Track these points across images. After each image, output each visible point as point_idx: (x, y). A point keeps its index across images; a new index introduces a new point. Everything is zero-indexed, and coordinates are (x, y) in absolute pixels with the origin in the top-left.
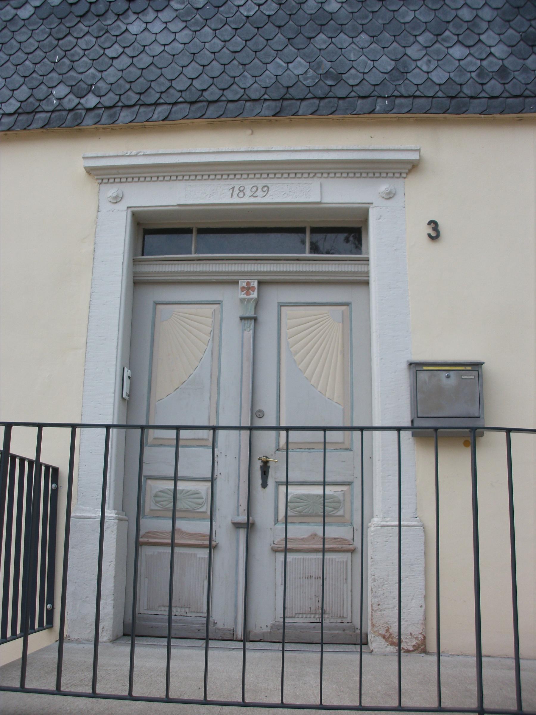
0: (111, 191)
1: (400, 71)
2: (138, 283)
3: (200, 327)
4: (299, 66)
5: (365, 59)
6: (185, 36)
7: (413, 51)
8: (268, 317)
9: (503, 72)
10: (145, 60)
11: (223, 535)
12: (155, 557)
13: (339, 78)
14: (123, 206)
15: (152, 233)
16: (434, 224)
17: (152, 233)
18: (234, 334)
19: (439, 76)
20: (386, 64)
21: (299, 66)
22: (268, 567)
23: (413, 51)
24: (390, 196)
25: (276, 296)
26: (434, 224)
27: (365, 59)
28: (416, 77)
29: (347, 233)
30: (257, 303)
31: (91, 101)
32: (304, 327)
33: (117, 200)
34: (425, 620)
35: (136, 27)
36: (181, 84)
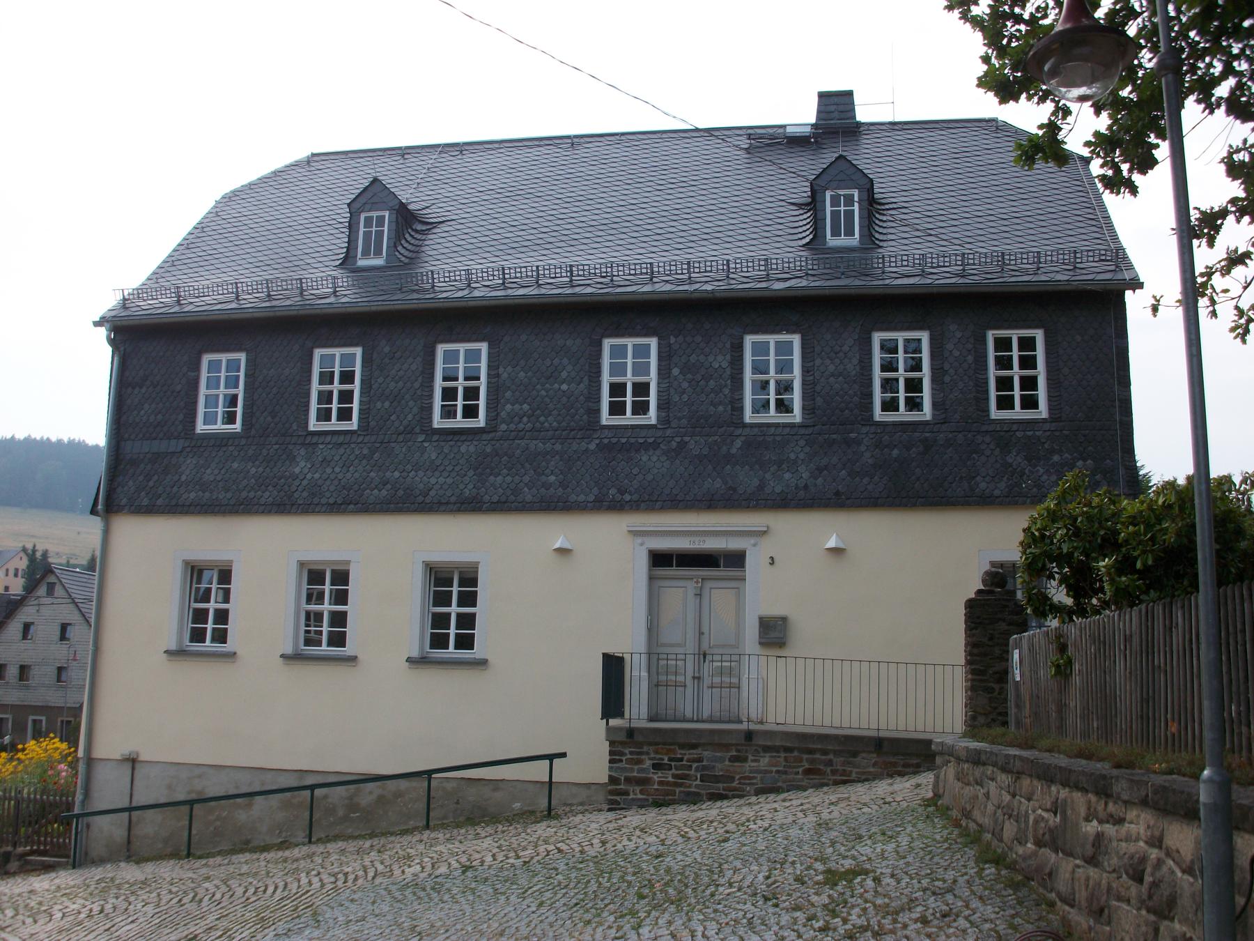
0: (639, 540)
1: (761, 487)
2: (651, 578)
3: (680, 591)
4: (718, 483)
5: (747, 479)
6: (667, 464)
7: (768, 476)
8: (706, 593)
9: (806, 487)
10: (650, 477)
11: (689, 682)
12: (654, 658)
13: (735, 490)
14: (644, 547)
15: (659, 559)
16: (772, 558)
17: (659, 559)
18: (692, 601)
19: (778, 489)
20: (756, 482)
21: (718, 483)
22: (707, 694)
23: (768, 476)
24: (754, 545)
25: (709, 584)
26: (772, 558)
27: (747, 479)
28: (768, 490)
29: (736, 560)
30: (701, 588)
31: (627, 497)
32: (720, 597)
33: (642, 544)
34: (129, 842)
35: (645, 458)
36: (667, 491)
